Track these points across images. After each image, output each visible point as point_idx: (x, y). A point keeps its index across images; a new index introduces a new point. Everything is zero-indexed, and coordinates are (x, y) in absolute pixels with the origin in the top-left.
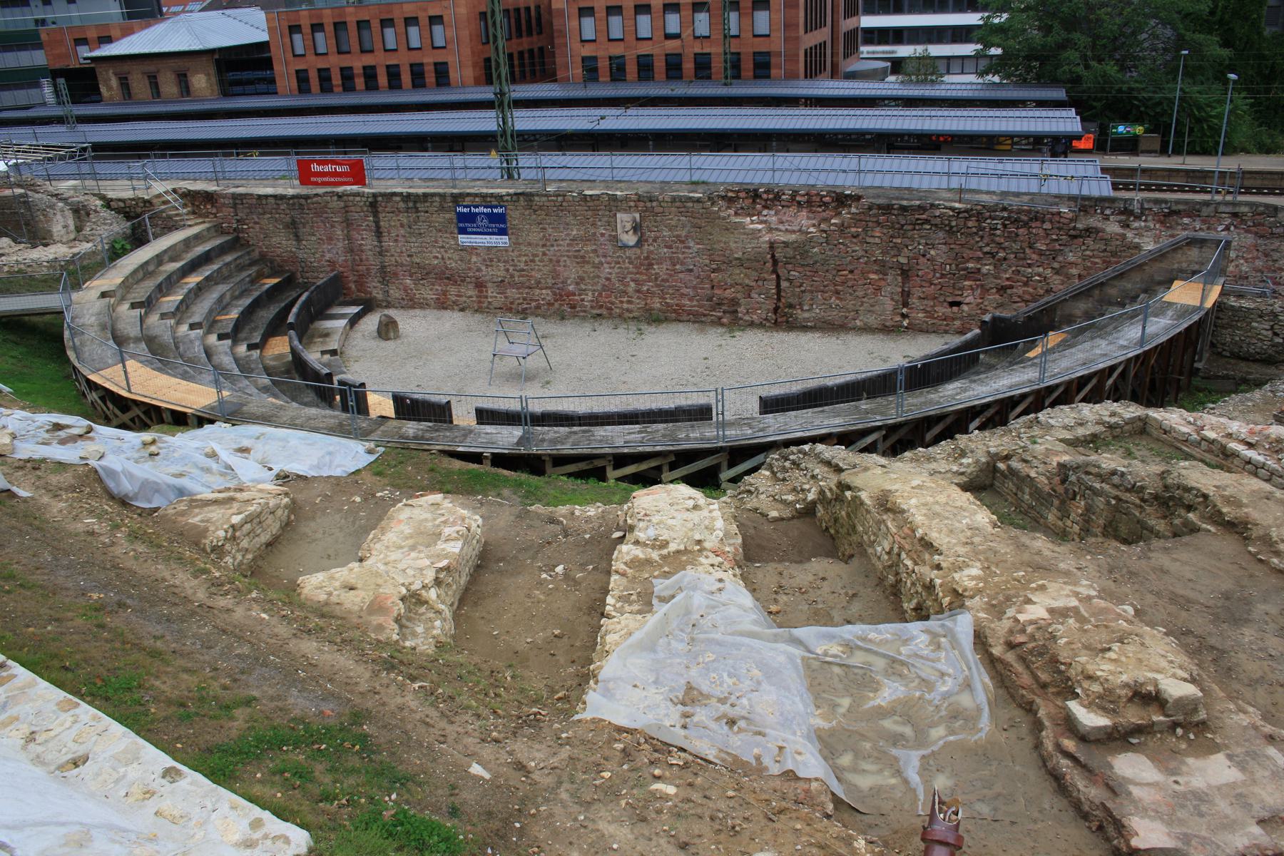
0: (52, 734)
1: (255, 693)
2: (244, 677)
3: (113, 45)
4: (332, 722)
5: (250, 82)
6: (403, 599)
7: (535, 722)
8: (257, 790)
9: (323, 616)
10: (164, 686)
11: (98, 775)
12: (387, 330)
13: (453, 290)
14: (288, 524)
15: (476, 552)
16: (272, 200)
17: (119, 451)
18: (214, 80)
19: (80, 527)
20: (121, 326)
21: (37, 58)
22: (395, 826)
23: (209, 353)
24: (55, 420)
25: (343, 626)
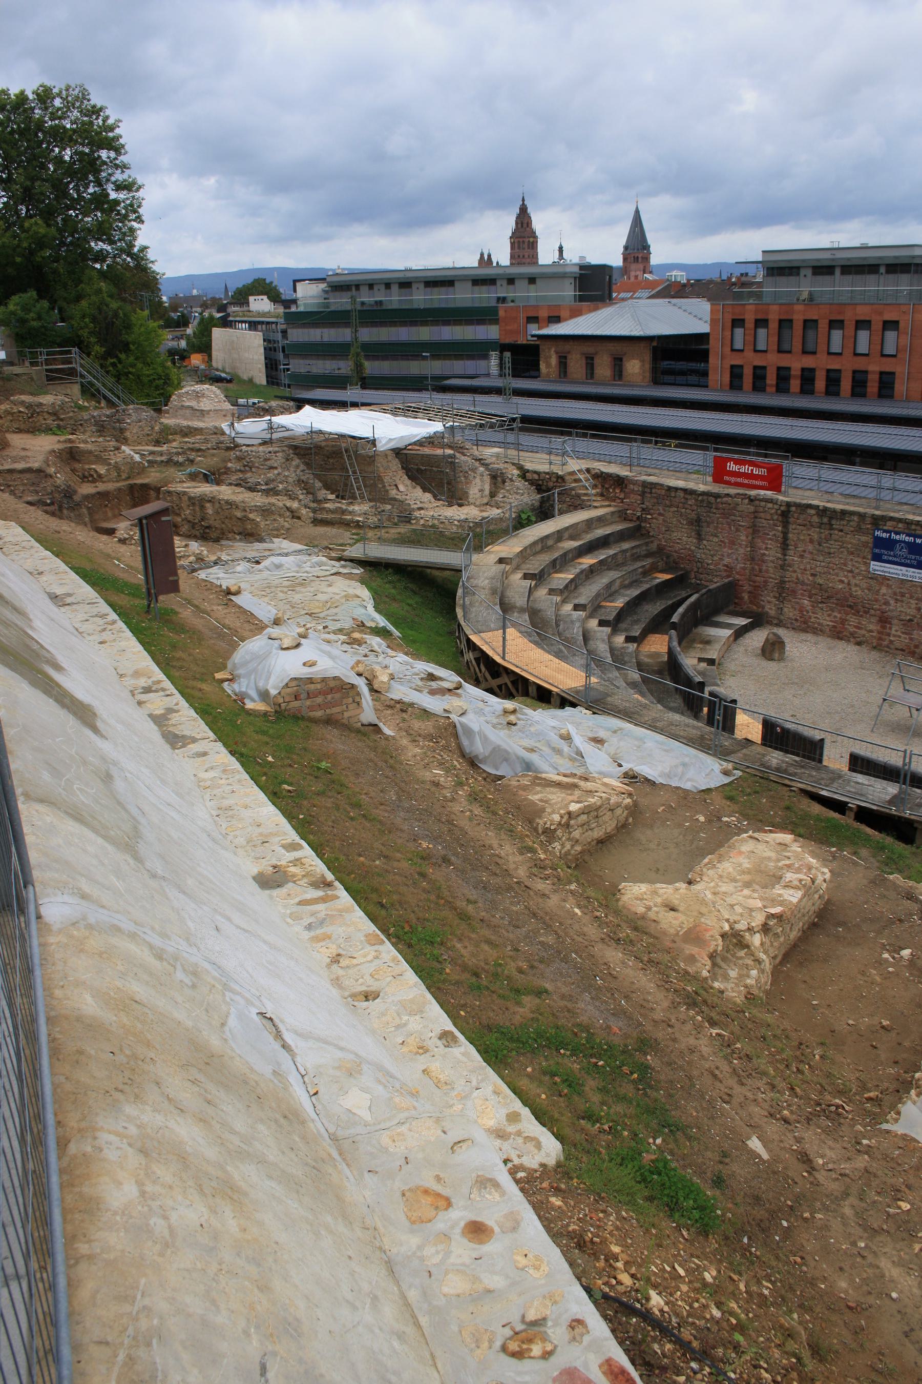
0: (355, 961)
1: (548, 986)
2: (542, 966)
3: (560, 325)
4: (616, 1040)
5: (683, 373)
6: (723, 936)
7: (836, 1115)
8: (524, 1083)
9: (636, 929)
10: (464, 950)
11: (383, 1014)
12: (772, 650)
13: (853, 620)
14: (624, 826)
15: (816, 908)
16: (681, 494)
17: (480, 712)
18: (648, 366)
19: (427, 775)
20: (509, 593)
21: (491, 332)
22: (652, 1173)
23: (586, 637)
24: (430, 670)
25: (654, 946)
